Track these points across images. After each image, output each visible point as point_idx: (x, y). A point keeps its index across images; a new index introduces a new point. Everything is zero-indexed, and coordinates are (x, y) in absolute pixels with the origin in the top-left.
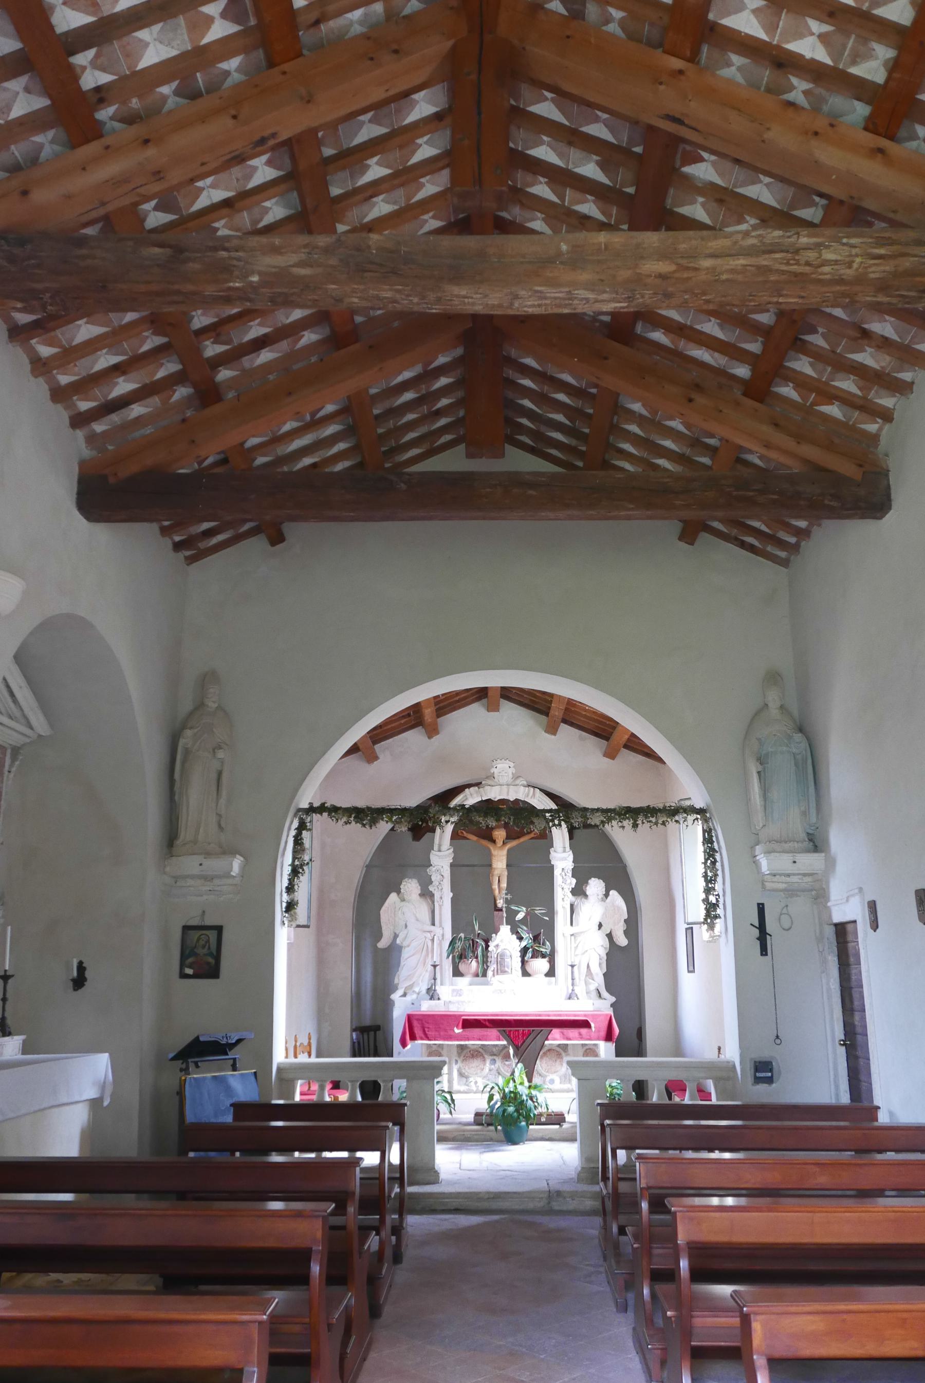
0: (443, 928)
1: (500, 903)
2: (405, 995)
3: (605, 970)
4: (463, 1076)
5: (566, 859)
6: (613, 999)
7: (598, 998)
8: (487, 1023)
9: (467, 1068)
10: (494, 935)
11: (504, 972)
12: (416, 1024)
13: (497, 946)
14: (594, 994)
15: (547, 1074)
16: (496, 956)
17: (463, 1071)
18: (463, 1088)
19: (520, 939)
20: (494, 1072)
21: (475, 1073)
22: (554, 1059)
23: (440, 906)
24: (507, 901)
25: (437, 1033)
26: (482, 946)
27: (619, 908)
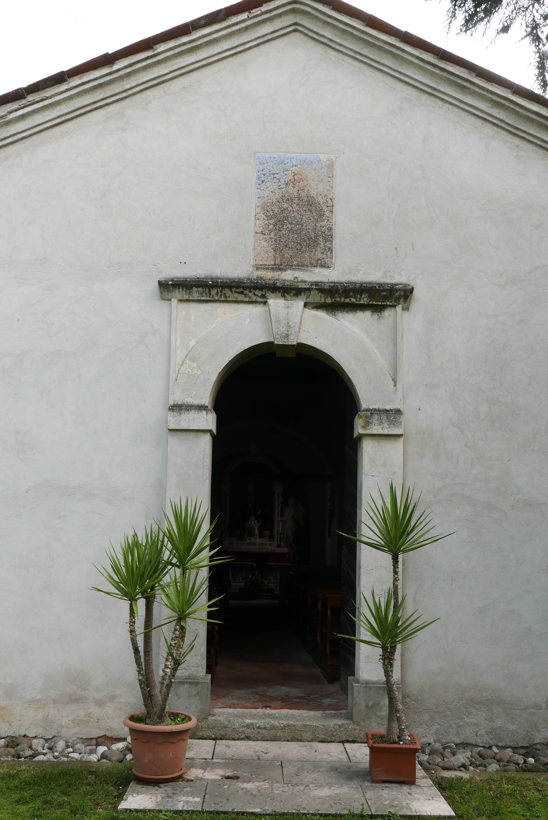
10: (331, 7)
19: (259, 522)
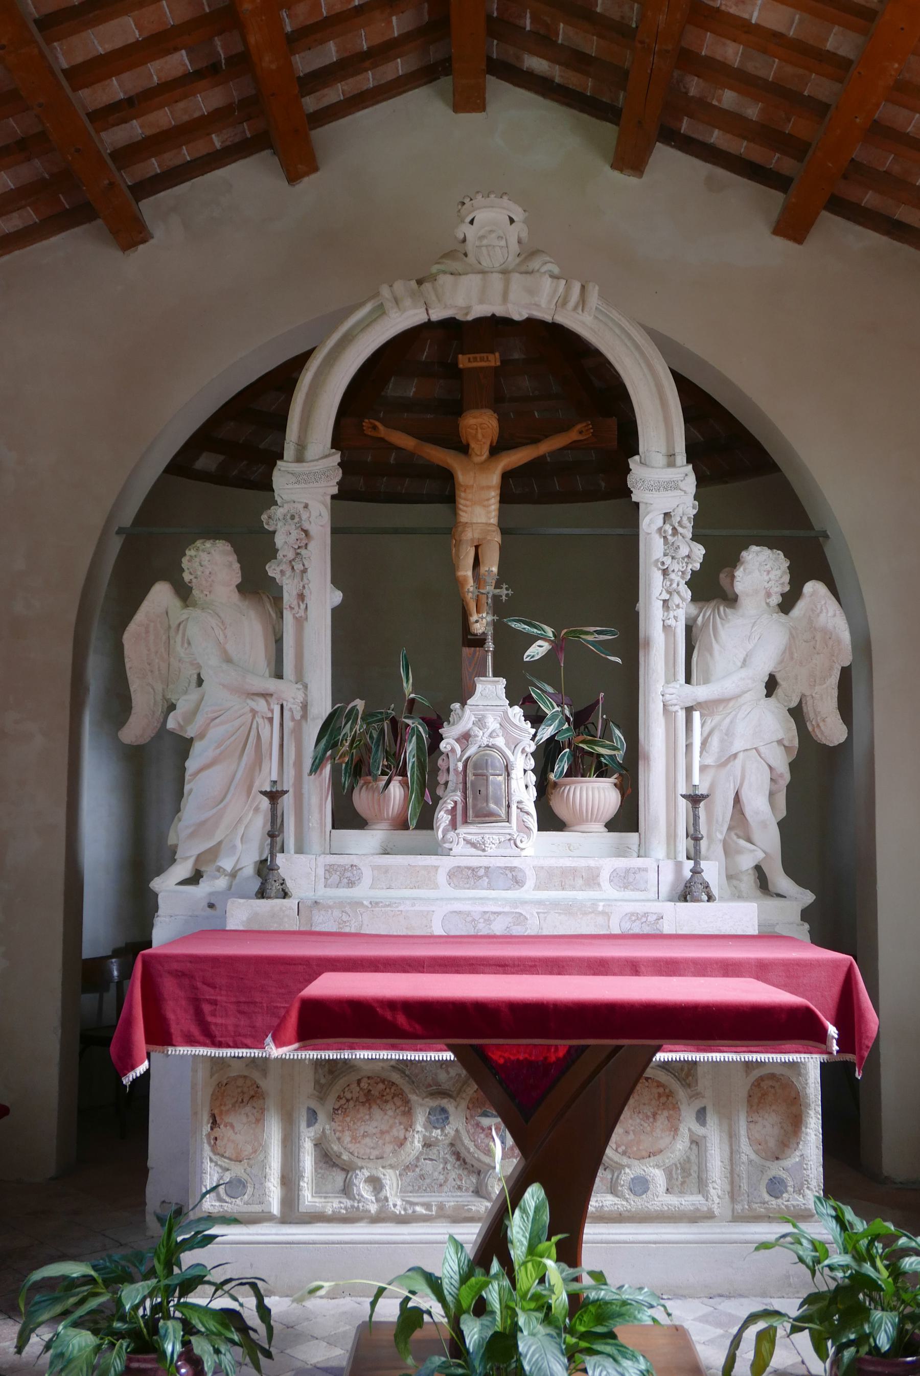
0: (306, 687)
1: (481, 623)
2: (195, 879)
3: (783, 813)
4: (335, 1165)
5: (677, 488)
6: (808, 897)
7: (759, 893)
8: (401, 1020)
9: (347, 1138)
10: (456, 706)
11: (485, 816)
12: (169, 987)
13: (465, 738)
14: (748, 882)
15: (625, 1161)
16: (460, 766)
17: (336, 1147)
18: (334, 1205)
19: (536, 719)
20: (443, 1151)
21: (375, 1153)
22: (648, 1111)
23: (300, 623)
24: (499, 608)
25: (243, 1021)
26: (419, 737)
27: (828, 635)
